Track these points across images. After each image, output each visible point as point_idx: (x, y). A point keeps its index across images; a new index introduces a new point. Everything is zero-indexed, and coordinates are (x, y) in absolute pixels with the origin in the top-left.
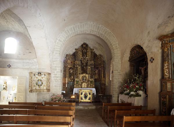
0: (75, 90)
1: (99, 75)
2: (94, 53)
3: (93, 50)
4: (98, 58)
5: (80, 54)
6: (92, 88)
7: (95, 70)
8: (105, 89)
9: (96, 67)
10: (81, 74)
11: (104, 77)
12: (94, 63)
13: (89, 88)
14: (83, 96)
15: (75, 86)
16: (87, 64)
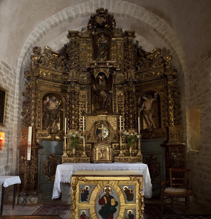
0: (62, 171)
1: (158, 116)
2: (136, 46)
3: (133, 35)
4: (151, 62)
5: (86, 49)
6: (133, 161)
7: (143, 100)
8: (182, 165)
9: (144, 90)
10: (88, 115)
11: (179, 122)
12: (136, 78)
13: (120, 161)
15: (65, 154)
16: (109, 81)
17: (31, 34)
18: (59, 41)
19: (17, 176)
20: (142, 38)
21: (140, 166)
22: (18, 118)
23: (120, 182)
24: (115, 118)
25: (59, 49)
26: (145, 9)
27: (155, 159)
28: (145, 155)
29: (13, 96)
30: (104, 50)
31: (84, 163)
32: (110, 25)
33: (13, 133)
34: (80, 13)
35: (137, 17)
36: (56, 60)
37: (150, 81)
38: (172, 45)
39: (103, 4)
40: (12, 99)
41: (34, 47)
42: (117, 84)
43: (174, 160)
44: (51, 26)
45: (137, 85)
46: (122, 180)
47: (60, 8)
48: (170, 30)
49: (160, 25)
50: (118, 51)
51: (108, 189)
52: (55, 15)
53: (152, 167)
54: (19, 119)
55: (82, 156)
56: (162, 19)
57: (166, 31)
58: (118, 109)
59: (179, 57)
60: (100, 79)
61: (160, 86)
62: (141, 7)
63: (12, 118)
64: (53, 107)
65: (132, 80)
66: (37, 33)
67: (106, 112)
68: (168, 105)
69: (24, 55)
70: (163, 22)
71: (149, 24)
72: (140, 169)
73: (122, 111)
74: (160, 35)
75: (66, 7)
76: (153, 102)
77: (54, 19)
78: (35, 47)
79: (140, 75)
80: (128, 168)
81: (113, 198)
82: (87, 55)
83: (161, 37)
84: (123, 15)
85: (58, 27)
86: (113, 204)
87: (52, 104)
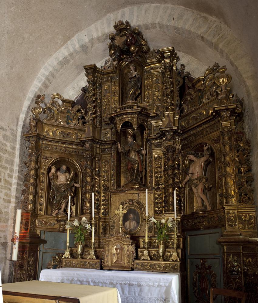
4: (201, 93)
9: (193, 145)
17: (36, 79)
18: (78, 85)
19: (12, 282)
20: (190, 59)
21: (160, 279)
22: (16, 199)
24: (151, 195)
25: (78, 97)
26: (185, 7)
27: (210, 267)
28: (195, 259)
29: (10, 168)
30: (133, 87)
31: (92, 268)
32: (138, 46)
33: (8, 219)
34: (95, 36)
35: (172, 23)
36: (69, 112)
37: (198, 126)
38: (231, 57)
39: (125, 15)
40: (8, 170)
42: (152, 139)
43: (234, 271)
44: (59, 64)
45: (182, 138)
47: (67, 34)
48: (226, 33)
49: (210, 28)
50: (154, 86)
52: (64, 47)
53: (204, 282)
54: (18, 200)
55: (143, 258)
56: (212, 17)
57: (221, 35)
58: (155, 180)
59: (244, 76)
60: (130, 133)
61: (214, 133)
62: (178, 6)
63: (6, 198)
64: (62, 180)
65: (169, 129)
66: (43, 77)
67: (137, 186)
68: (227, 165)
69: (26, 109)
70: (215, 22)
71: (192, 29)
72: (161, 286)
73: (161, 183)
74: (211, 44)
75: (77, 32)
76: (206, 163)
77: (63, 52)
78: (38, 96)
79: (187, 119)
80: (141, 282)
82: (111, 98)
83: (214, 47)
84: (154, 26)
85: (70, 63)
87: (60, 177)
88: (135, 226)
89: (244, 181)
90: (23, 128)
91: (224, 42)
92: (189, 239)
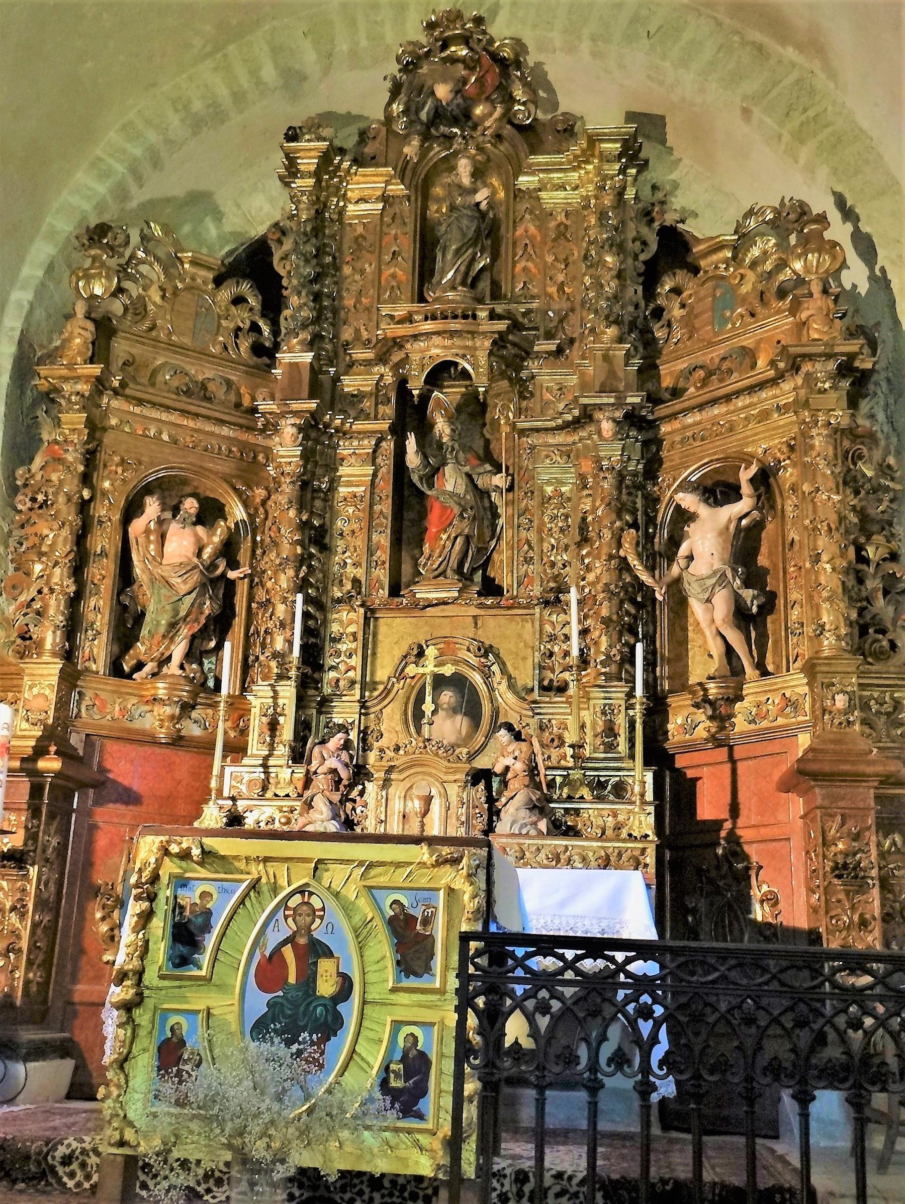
14: (224, 1001)
23: (373, 872)
25: (236, 249)
41: (92, 226)
44: (188, 122)
46: (382, 864)
48: (830, 108)
49: (775, 84)
51: (308, 903)
53: (730, 924)
57: (811, 113)
69: (40, 273)
81: (329, 954)
86: (326, 987)
88: (464, 732)
89: (875, 590)
90: (20, 342)
91: (820, 137)
92: (668, 780)
